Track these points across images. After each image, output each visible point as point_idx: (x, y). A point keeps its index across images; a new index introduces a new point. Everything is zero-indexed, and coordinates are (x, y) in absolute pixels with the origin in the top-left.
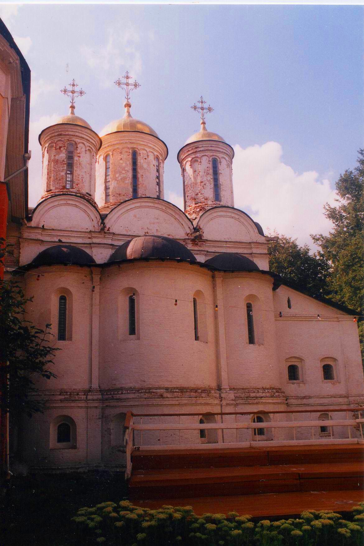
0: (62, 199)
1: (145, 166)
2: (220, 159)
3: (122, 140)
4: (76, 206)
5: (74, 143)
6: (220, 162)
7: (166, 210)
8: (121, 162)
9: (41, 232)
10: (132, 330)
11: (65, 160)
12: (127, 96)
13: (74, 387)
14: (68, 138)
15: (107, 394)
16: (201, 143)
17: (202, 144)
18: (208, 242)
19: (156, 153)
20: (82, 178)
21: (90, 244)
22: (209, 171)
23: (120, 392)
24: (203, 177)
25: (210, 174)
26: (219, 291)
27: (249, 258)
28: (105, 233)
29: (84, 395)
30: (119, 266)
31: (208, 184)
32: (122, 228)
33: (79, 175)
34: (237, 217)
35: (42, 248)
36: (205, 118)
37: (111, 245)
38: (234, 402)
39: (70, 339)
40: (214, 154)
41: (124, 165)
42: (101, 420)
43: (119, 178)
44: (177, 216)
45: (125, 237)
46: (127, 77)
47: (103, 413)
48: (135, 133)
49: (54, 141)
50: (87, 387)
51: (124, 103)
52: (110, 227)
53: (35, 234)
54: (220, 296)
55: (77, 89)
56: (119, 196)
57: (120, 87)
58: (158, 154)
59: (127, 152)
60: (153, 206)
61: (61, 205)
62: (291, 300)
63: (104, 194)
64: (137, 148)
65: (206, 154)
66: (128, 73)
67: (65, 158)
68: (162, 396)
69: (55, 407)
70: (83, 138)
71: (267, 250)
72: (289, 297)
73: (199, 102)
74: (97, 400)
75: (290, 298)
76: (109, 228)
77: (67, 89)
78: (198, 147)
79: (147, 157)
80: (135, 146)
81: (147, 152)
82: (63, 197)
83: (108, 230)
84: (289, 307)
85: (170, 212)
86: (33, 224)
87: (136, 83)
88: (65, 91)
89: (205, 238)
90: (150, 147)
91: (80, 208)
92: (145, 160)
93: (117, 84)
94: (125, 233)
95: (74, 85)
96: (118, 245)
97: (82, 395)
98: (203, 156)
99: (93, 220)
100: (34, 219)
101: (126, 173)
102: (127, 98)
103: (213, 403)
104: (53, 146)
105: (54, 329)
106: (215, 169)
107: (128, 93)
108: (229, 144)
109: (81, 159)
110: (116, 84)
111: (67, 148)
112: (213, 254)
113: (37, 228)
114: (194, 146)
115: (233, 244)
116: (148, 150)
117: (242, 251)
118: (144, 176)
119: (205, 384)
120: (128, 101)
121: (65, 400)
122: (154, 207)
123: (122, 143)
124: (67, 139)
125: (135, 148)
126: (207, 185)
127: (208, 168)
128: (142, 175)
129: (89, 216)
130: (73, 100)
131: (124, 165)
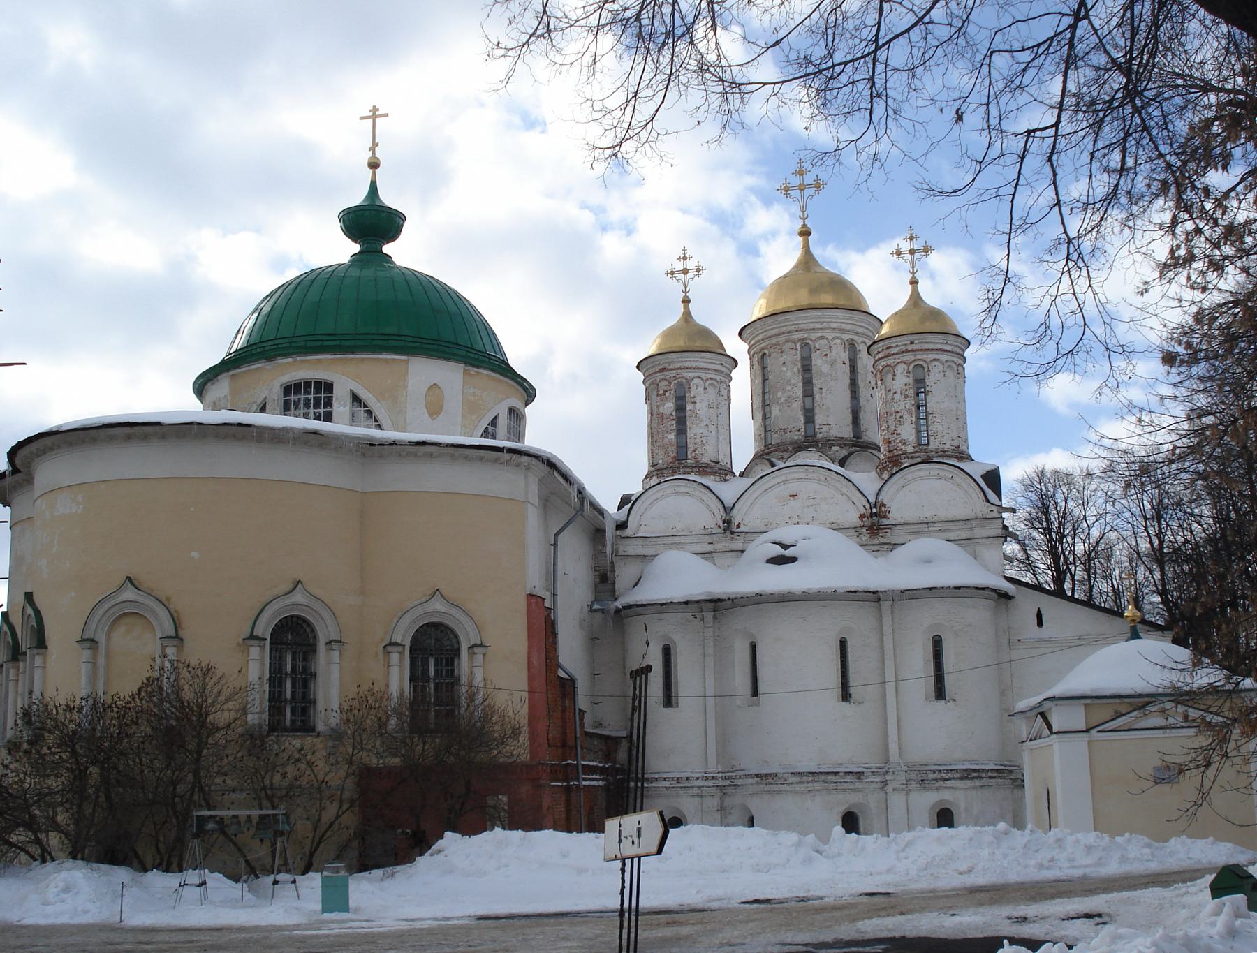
1: (825, 368)
5: (684, 381)
6: (929, 371)
8: (784, 369)
11: (674, 414)
16: (893, 340)
26: (887, 620)
28: (732, 533)
31: (906, 416)
32: (759, 521)
41: (789, 374)
43: (783, 399)
54: (887, 628)
58: (851, 337)
78: (890, 347)
80: (806, 335)
84: (1040, 624)
88: (672, 273)
92: (824, 358)
93: (783, 192)
95: (685, 258)
114: (884, 346)
118: (824, 390)
125: (803, 339)
126: (905, 417)
130: (686, 288)
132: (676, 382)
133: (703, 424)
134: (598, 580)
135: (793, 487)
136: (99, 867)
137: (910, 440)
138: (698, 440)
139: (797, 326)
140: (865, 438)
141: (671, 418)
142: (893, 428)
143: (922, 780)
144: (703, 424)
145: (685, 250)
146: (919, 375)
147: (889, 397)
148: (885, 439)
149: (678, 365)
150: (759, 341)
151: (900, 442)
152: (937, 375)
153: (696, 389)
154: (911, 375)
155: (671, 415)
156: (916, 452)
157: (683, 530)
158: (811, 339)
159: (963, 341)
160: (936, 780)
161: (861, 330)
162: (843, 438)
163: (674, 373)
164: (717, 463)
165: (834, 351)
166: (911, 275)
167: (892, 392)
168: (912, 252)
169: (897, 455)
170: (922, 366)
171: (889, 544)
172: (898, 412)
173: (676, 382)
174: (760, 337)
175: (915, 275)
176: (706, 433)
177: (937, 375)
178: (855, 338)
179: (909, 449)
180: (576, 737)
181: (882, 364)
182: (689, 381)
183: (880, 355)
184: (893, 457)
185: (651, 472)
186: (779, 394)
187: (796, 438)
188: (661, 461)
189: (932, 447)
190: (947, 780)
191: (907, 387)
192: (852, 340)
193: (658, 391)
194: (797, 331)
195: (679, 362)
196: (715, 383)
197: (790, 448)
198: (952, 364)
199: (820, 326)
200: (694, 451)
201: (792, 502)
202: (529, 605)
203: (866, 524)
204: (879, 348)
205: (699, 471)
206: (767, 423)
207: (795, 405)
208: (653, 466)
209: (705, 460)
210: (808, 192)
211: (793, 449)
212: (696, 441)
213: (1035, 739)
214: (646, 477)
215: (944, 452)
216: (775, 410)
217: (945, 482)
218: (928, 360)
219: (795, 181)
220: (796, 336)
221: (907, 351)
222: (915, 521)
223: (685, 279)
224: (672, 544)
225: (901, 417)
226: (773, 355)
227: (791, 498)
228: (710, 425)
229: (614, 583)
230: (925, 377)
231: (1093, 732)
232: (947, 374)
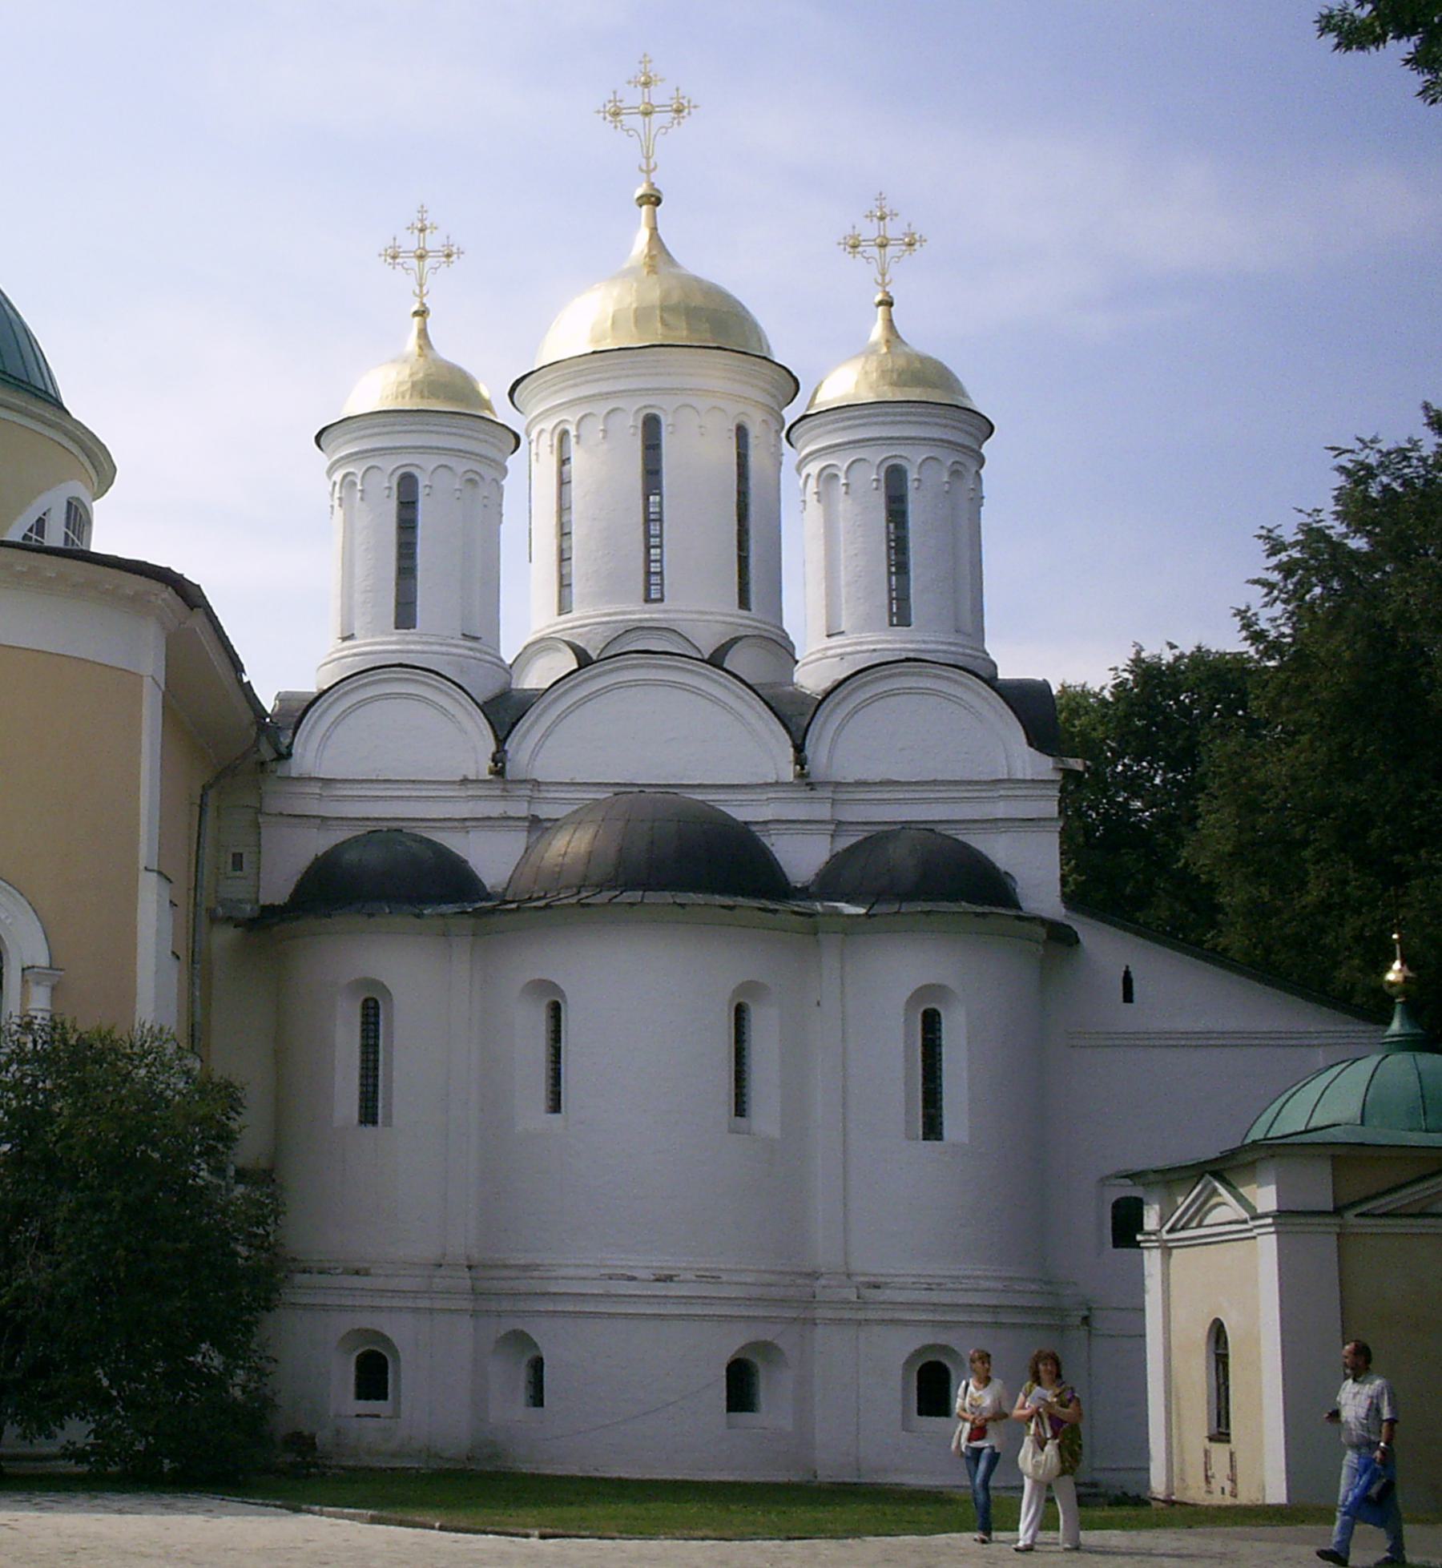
9: (318, 791)
12: (644, 160)
27: (960, 837)
36: (890, 281)
39: (388, 1123)
51: (640, 191)
57: (619, 125)
62: (1133, 975)
66: (650, 61)
69: (342, 1308)
72: (1127, 967)
73: (870, 216)
75: (1130, 969)
84: (1128, 997)
87: (678, 98)
100: (297, 749)
102: (644, 168)
106: (895, 506)
108: (365, 816)
110: (605, 119)
120: (648, 181)
130: (421, 286)
145: (422, 210)
159: (977, 421)
213: (1183, 1228)
231: (1349, 1216)
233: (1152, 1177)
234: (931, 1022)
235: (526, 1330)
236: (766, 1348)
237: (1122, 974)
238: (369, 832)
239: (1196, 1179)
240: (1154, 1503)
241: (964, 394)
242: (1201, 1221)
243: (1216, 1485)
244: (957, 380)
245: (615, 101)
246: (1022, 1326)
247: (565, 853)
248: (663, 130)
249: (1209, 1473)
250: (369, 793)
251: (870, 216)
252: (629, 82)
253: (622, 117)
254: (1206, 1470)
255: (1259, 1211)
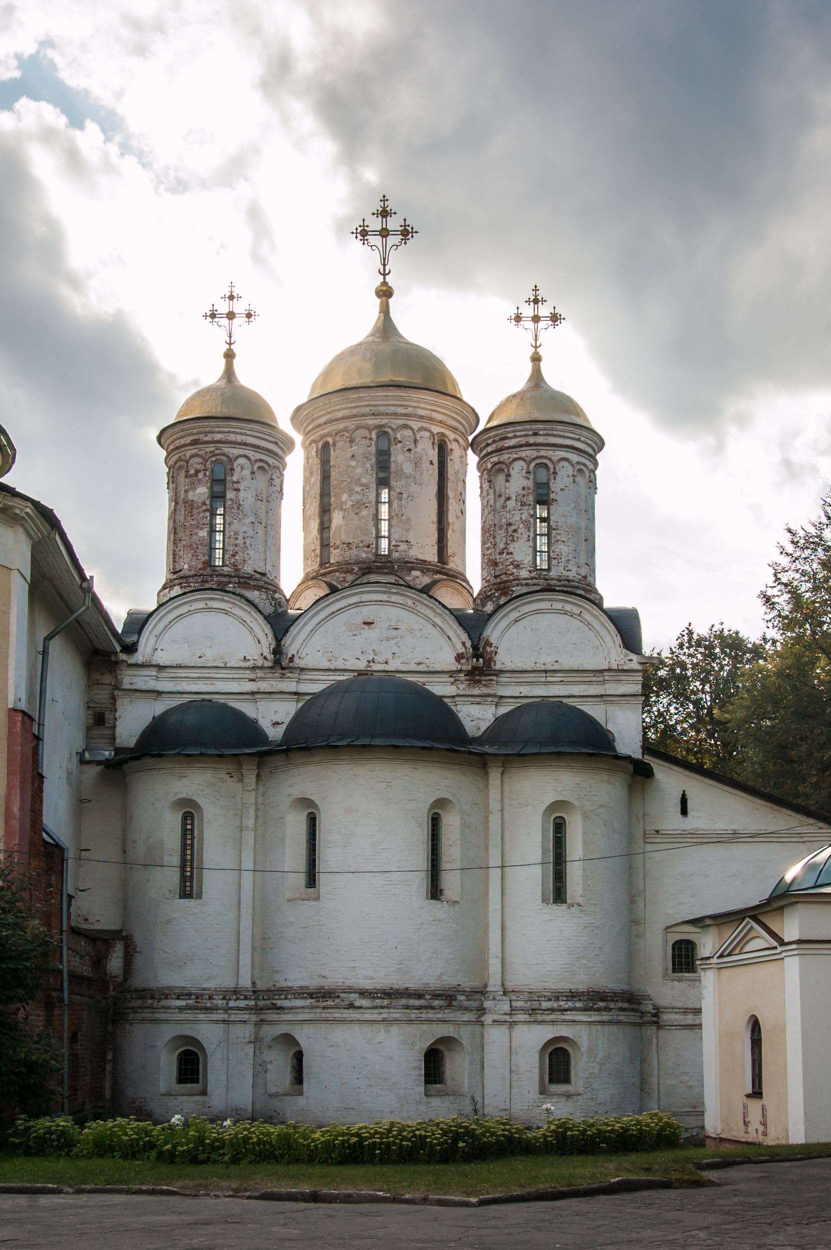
0: (196, 600)
1: (408, 468)
2: (554, 464)
3: (355, 407)
4: (226, 612)
6: (555, 473)
7: (414, 606)
8: (353, 463)
10: (435, 822)
13: (205, 985)
14: (212, 449)
15: (264, 999)
17: (514, 431)
18: (504, 675)
19: (436, 429)
20: (244, 538)
21: (253, 693)
22: (525, 498)
23: (283, 997)
24: (512, 513)
25: (530, 505)
29: (224, 999)
30: (287, 756)
32: (320, 654)
33: (236, 533)
34: (577, 610)
35: (160, 707)
37: (295, 693)
38: (507, 1018)
39: (200, 896)
40: (543, 453)
42: (253, 1046)
43: (349, 503)
44: (438, 620)
45: (326, 674)
46: (384, 213)
47: (257, 1033)
48: (382, 388)
49: (185, 455)
50: (229, 984)
52: (295, 653)
53: (145, 678)
55: (239, 307)
56: (347, 549)
57: (366, 242)
59: (365, 438)
60: (386, 601)
61: (197, 611)
63: (318, 542)
64: (389, 425)
65: (523, 454)
66: (387, 200)
67: (208, 498)
68: (351, 1006)
69: (167, 1021)
70: (245, 444)
71: (640, 685)
72: (684, 791)
73: (528, 301)
74: (246, 1009)
75: (686, 793)
76: (293, 655)
77: (216, 311)
79: (414, 444)
80: (384, 422)
81: (414, 434)
82: (198, 596)
83: (291, 660)
84: (684, 812)
85: (424, 613)
86: (139, 657)
87: (405, 226)
88: (213, 316)
89: (498, 666)
90: (422, 417)
91: (234, 616)
92: (407, 453)
93: (359, 237)
94: (326, 665)
95: (231, 298)
96: (311, 691)
97: (219, 999)
98: (515, 459)
99: (259, 641)
100: (141, 647)
101: (363, 490)
102: (382, 272)
103: (460, 1019)
104: (180, 468)
105: (170, 877)
107: (384, 259)
109: (242, 494)
110: (356, 237)
111: (212, 472)
112: (512, 700)
113: (143, 666)
114: (496, 436)
115: (562, 675)
116: (416, 425)
117: (584, 689)
118: (405, 496)
119: (444, 983)
121: (188, 1008)
122: (389, 602)
123: (355, 416)
124: (211, 452)
125: (383, 426)
126: (520, 531)
127: (524, 489)
128: (401, 493)
129: (251, 630)
131: (359, 470)
132: (214, 459)
133: (247, 521)
134: (91, 721)
135: (367, 613)
136: (574, 1037)
137: (526, 562)
138: (240, 541)
139: (373, 409)
140: (451, 565)
141: (204, 508)
142: (502, 546)
143: (533, 1010)
144: (248, 521)
146: (542, 475)
147: (498, 506)
148: (489, 560)
149: (218, 437)
150: (320, 425)
151: (512, 563)
152: (565, 479)
153: (242, 471)
154: (531, 477)
155: (204, 504)
156: (532, 578)
157: (214, 660)
158: (390, 427)
160: (552, 1010)
161: (454, 424)
162: (426, 561)
163: (210, 448)
164: (264, 575)
165: (420, 446)
166: (534, 350)
167: (503, 498)
168: (536, 319)
169: (507, 581)
170: (546, 466)
171: (494, 696)
172: (510, 524)
173: (214, 459)
174: (323, 420)
175: (538, 350)
176: (250, 533)
177: (565, 479)
178: (447, 432)
179: (524, 574)
180: (62, 931)
181: (492, 460)
182: (231, 460)
183: (489, 449)
184: (500, 583)
185: (171, 581)
186: (345, 497)
187: (364, 555)
188: (186, 567)
189: (553, 573)
190: (566, 1010)
191: (525, 492)
192: (443, 434)
193: (187, 471)
194: (373, 414)
195: (219, 432)
196: (265, 466)
197: (356, 569)
198: (583, 468)
199: (404, 411)
200: (234, 556)
201: (367, 632)
202: (11, 723)
203: (464, 668)
204: (490, 438)
205: (239, 583)
206: (325, 535)
207: (364, 512)
208: (175, 573)
209: (248, 569)
210: (392, 240)
211: (360, 569)
212: (237, 542)
213: (729, 955)
214: (164, 588)
215: (569, 581)
216: (337, 518)
217: (572, 619)
218: (555, 459)
219: (375, 224)
220: (371, 422)
221: (528, 445)
222: (529, 668)
223: (385, 247)
224: (199, 678)
225: (515, 531)
226: (338, 445)
227: (366, 627)
228: (256, 523)
229: (114, 727)
230: (549, 480)
232: (577, 479)
233: (708, 922)
234: (559, 827)
235: (292, 1033)
236: (447, 1041)
237: (681, 796)
238: (190, 701)
239: (740, 922)
240: (708, 1142)
241: (586, 420)
242: (742, 948)
243: (751, 1129)
244: (582, 410)
245: (364, 226)
246: (590, 1023)
247: (320, 714)
248: (395, 247)
249: (747, 1120)
250: (191, 675)
251: (528, 301)
252: (373, 214)
253: (368, 237)
254: (744, 1118)
255: (786, 941)
